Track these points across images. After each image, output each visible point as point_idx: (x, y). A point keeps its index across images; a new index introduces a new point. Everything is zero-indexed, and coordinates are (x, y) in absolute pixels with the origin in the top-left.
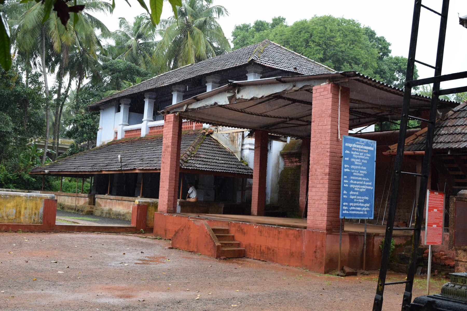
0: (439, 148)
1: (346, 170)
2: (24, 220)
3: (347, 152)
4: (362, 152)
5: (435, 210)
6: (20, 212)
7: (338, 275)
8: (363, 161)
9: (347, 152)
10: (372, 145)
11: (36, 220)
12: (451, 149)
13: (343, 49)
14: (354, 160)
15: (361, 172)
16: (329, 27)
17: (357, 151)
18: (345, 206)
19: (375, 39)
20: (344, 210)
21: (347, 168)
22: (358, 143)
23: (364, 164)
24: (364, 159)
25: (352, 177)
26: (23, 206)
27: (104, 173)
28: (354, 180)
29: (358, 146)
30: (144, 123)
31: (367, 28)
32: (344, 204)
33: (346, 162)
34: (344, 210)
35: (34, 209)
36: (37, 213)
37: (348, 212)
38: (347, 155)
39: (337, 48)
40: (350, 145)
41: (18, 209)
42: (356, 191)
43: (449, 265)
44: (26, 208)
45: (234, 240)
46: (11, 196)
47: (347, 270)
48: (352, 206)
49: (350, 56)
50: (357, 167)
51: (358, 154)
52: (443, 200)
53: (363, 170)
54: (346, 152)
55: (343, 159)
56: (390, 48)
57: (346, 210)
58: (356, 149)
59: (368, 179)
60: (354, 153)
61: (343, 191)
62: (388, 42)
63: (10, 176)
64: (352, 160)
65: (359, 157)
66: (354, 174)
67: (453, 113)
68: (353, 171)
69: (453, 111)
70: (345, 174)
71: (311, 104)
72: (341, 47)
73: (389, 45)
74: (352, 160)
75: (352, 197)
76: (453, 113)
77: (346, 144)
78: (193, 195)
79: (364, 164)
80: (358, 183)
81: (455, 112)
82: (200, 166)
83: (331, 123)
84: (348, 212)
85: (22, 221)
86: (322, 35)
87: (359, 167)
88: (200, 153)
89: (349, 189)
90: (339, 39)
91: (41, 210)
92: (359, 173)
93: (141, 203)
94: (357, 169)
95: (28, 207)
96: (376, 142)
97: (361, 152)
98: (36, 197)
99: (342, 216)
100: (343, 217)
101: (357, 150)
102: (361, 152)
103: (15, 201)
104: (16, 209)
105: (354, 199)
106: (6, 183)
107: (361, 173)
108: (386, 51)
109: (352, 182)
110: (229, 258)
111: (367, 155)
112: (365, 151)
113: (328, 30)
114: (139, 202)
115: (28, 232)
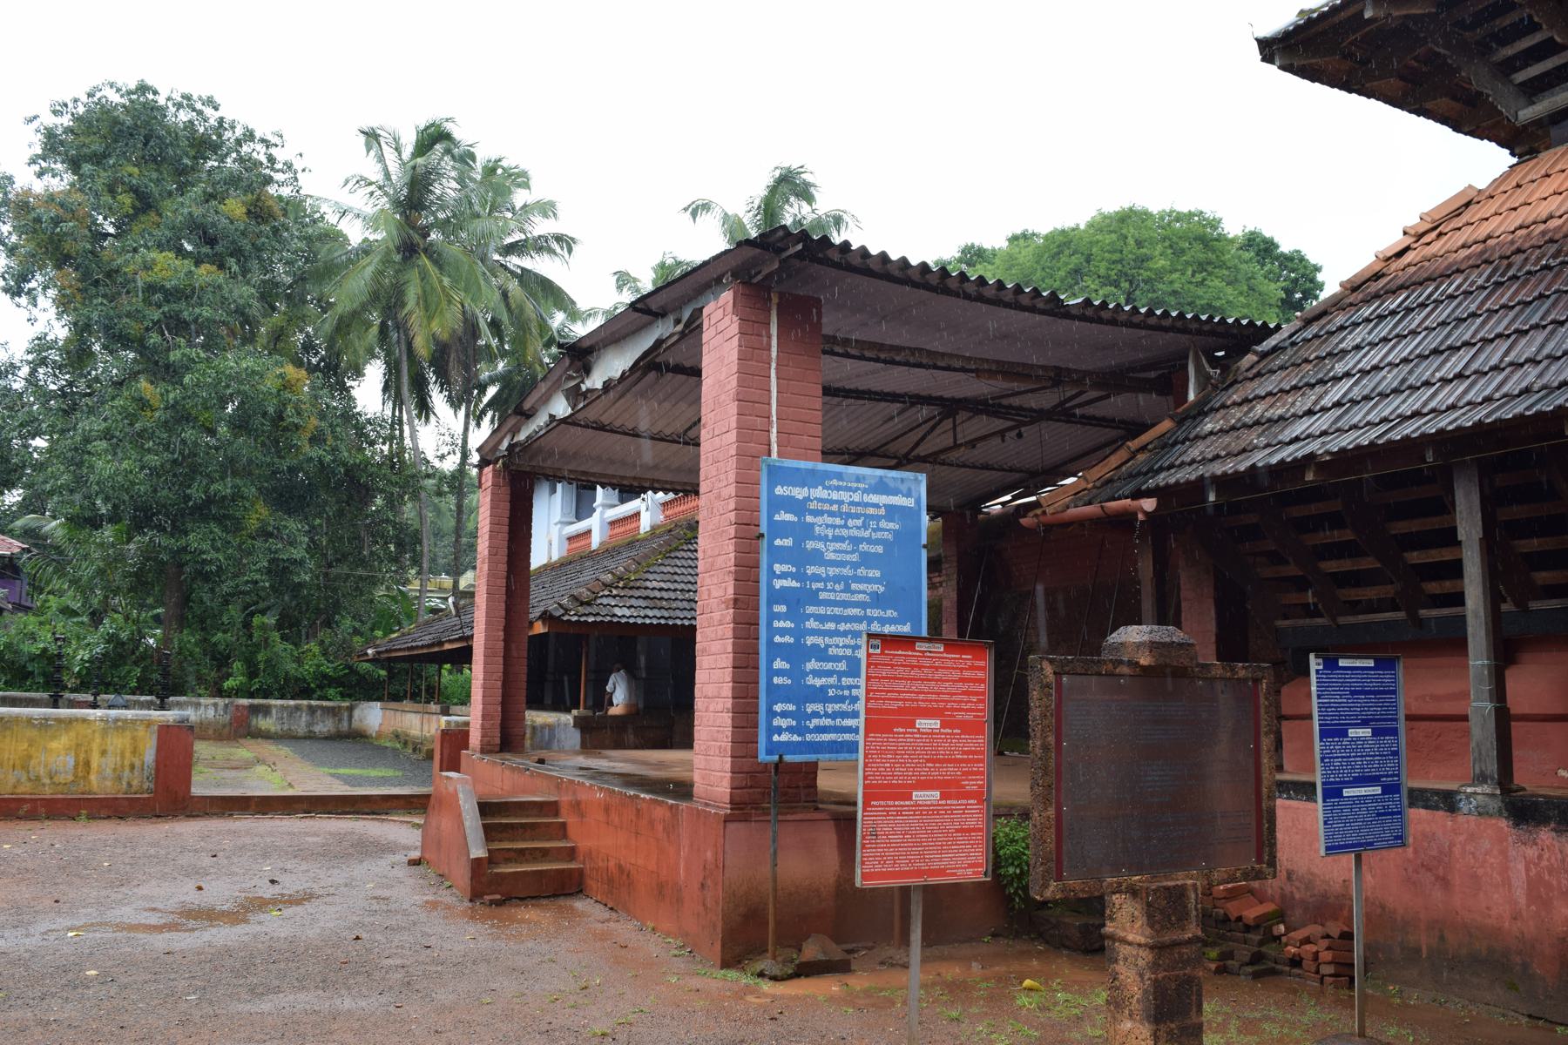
0: (1177, 483)
1: (778, 584)
2: (100, 783)
3: (785, 517)
4: (857, 516)
5: (924, 724)
6: (87, 764)
7: (761, 975)
8: (864, 547)
9: (785, 517)
10: (904, 488)
11: (135, 783)
12: (1222, 482)
13: (1177, 286)
14: (820, 545)
15: (854, 586)
16: (1131, 232)
17: (831, 514)
18: (784, 714)
19: (1277, 258)
20: (779, 731)
21: (784, 576)
22: (835, 482)
23: (867, 560)
24: (869, 541)
25: (811, 610)
26: (95, 746)
27: (447, 646)
28: (822, 619)
29: (835, 496)
30: (596, 515)
31: (1252, 233)
32: (778, 708)
33: (778, 555)
34: (779, 731)
35: (128, 754)
36: (137, 763)
37: (796, 738)
38: (780, 529)
39: (1161, 286)
40: (799, 493)
41: (82, 756)
42: (837, 659)
43: (1240, 919)
44: (104, 753)
45: (565, 836)
46: (59, 720)
47: (812, 951)
48: (816, 715)
49: (1198, 302)
50: (832, 571)
51: (838, 521)
52: (980, 674)
53: (867, 580)
54: (777, 517)
55: (764, 543)
56: (1320, 277)
57: (790, 729)
58: (826, 507)
59: (890, 613)
60: (819, 520)
61: (770, 662)
62: (1313, 261)
63: (328, 669)
64: (810, 545)
65: (845, 532)
66: (823, 596)
67: (1255, 358)
68: (820, 585)
69: (1256, 353)
70: (776, 597)
71: (697, 372)
72: (1171, 282)
73: (1317, 269)
74: (810, 545)
75: (818, 682)
76: (1255, 358)
77: (779, 490)
78: (620, 695)
79: (867, 560)
80: (843, 627)
81: (1264, 356)
82: (627, 612)
83: (738, 421)
84: (796, 738)
85: (95, 789)
86: (1116, 256)
87: (847, 571)
88: (651, 577)
89: (797, 654)
90: (1162, 262)
91: (149, 755)
92: (847, 589)
93: (453, 726)
94: (837, 579)
95: (110, 748)
96: (923, 478)
97: (849, 516)
98: (133, 722)
99: (769, 752)
100: (776, 758)
101: (835, 508)
102: (849, 516)
103: (72, 734)
104: (77, 756)
105: (823, 688)
106: (321, 687)
107: (853, 592)
108: (1308, 285)
109: (812, 624)
110: (522, 899)
111: (883, 524)
112: (871, 511)
113: (1131, 241)
114: (448, 723)
115: (109, 817)
